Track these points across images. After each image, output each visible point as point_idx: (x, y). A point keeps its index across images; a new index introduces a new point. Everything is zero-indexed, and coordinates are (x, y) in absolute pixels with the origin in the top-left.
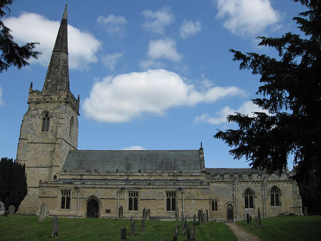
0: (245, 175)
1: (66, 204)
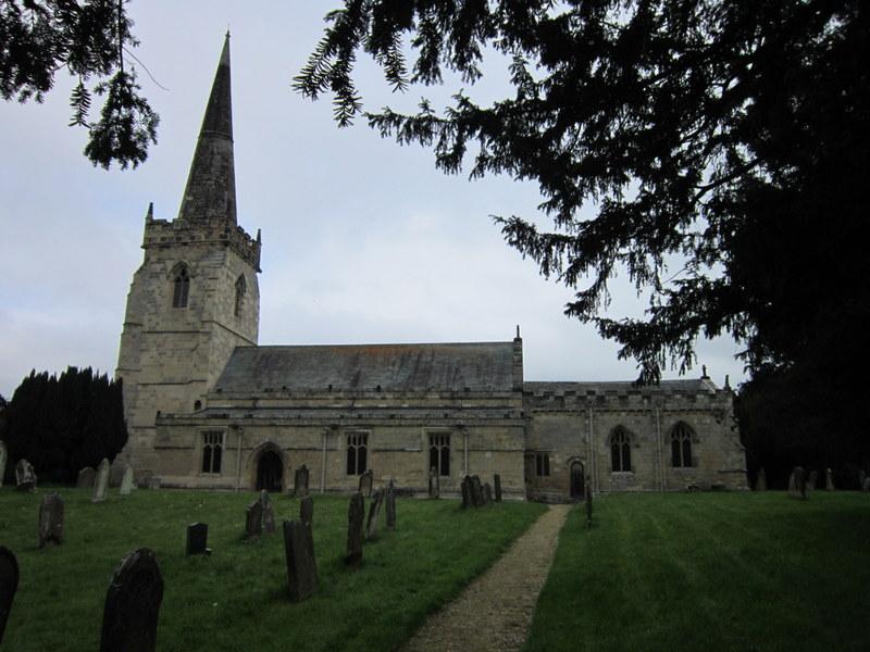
0: (612, 398)
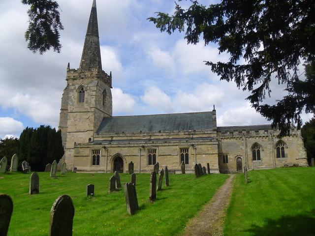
1: (96, 161)
